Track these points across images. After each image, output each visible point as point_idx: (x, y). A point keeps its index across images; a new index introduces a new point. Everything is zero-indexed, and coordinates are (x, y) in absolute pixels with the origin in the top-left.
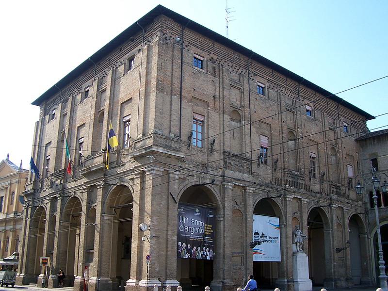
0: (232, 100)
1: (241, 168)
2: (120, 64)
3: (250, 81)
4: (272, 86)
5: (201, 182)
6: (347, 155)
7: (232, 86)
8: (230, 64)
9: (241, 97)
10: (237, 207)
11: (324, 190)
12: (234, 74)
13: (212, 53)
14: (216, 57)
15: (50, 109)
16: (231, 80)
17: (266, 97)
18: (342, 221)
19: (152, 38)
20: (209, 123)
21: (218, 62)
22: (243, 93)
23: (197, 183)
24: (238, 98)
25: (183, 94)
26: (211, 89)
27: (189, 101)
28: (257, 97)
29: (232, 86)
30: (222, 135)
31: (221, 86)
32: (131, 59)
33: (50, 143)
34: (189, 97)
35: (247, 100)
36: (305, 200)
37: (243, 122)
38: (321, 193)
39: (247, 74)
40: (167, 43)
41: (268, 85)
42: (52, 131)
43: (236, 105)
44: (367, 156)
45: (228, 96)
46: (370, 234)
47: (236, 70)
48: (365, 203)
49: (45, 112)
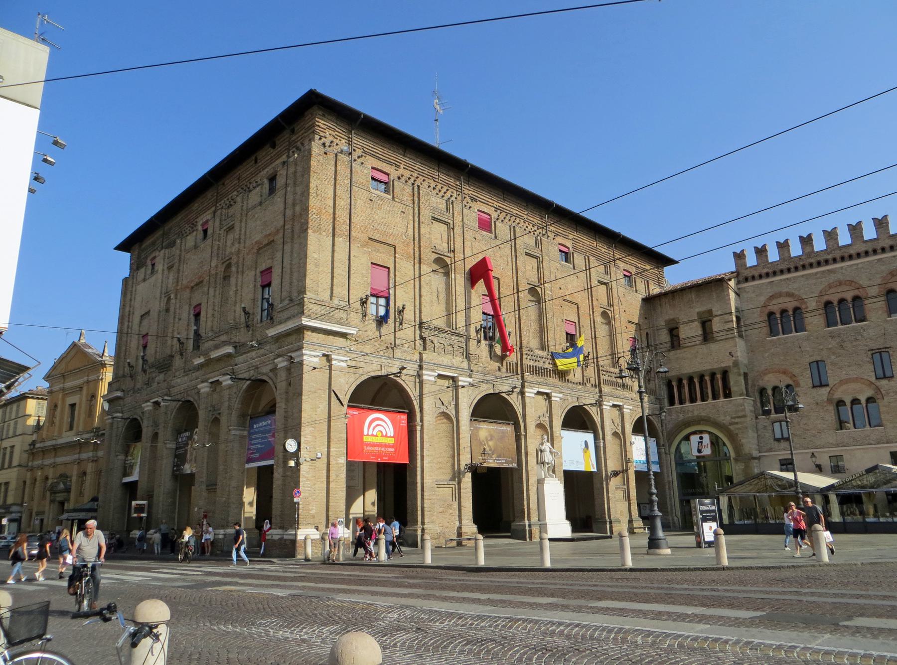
0: (436, 241)
1: (450, 348)
2: (255, 184)
3: (465, 210)
4: (501, 217)
5: (384, 372)
6: (629, 322)
7: (434, 219)
8: (433, 184)
9: (449, 235)
10: (443, 409)
11: (589, 380)
12: (439, 200)
13: (402, 166)
14: (410, 173)
15: (146, 258)
16: (434, 209)
17: (493, 235)
18: (620, 428)
19: (302, 144)
20: (397, 279)
21: (412, 180)
22: (453, 229)
23: (379, 373)
24: (445, 237)
25: (353, 234)
26: (400, 225)
27: (365, 245)
28: (477, 235)
29: (434, 219)
30: (417, 280)
31: (416, 219)
32: (272, 179)
33: (148, 313)
34: (364, 237)
35: (459, 240)
36: (556, 397)
38: (583, 384)
39: (459, 198)
40: (326, 153)
41: (496, 216)
42: (149, 291)
43: (441, 249)
44: (663, 323)
45: (427, 236)
46: (670, 447)
47: (441, 194)
49: (136, 266)
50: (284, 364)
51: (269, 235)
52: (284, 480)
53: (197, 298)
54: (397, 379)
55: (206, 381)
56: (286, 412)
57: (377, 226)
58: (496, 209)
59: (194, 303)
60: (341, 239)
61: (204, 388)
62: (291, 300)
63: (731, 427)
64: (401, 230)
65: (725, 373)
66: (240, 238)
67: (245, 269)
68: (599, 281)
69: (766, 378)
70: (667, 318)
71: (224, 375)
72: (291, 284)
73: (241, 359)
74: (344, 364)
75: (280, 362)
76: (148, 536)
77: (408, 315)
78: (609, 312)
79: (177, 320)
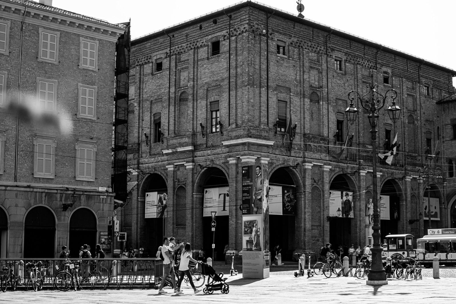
26: (292, 74)
45: (308, 80)
46: (448, 205)
50: (234, 162)
51: (217, 80)
52: (236, 225)
53: (156, 109)
54: (294, 170)
55: (172, 164)
56: (236, 188)
57: (281, 78)
58: (346, 54)
59: (154, 111)
60: (264, 89)
61: (170, 168)
62: (237, 125)
64: (293, 77)
66: (194, 78)
67: (198, 98)
68: (408, 95)
70: (452, 117)
71: (187, 162)
72: (236, 115)
73: (198, 153)
74: (267, 162)
75: (231, 160)
76: (240, 254)
77: (298, 130)
78: (414, 115)
79: (141, 120)
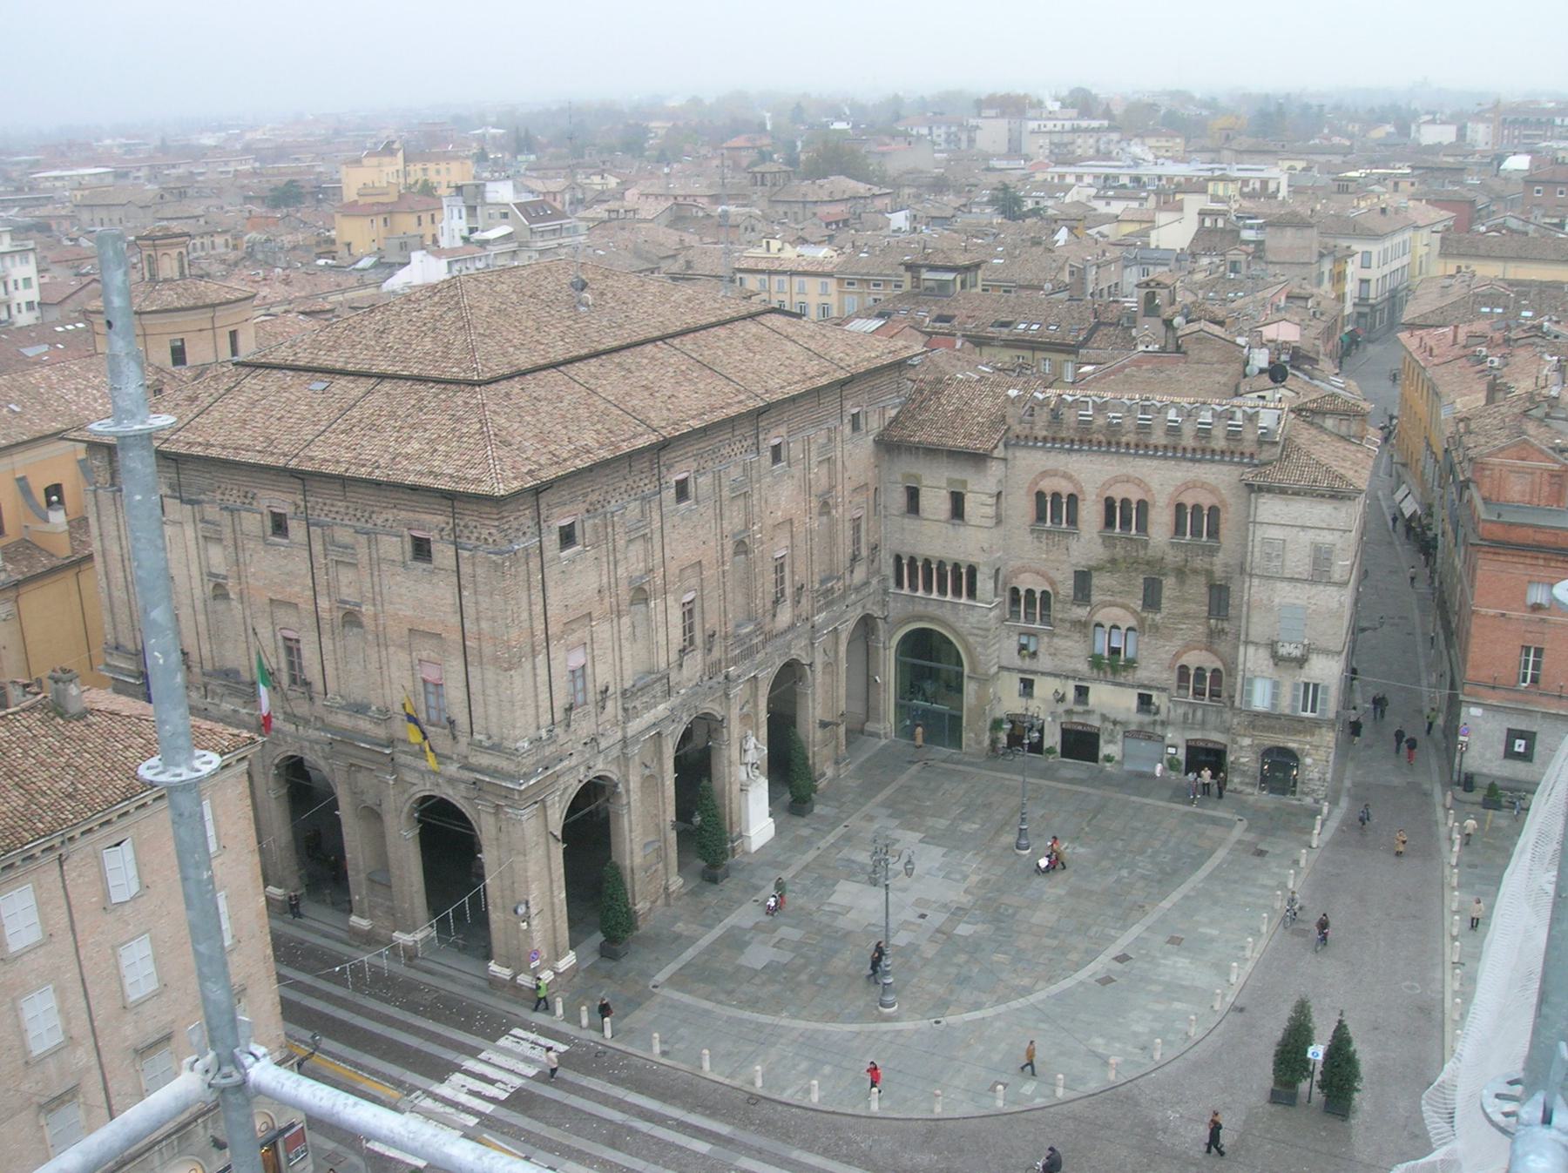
9: (646, 550)
37: (652, 604)
48: (884, 579)
63: (971, 639)
65: (972, 571)
69: (1022, 576)
